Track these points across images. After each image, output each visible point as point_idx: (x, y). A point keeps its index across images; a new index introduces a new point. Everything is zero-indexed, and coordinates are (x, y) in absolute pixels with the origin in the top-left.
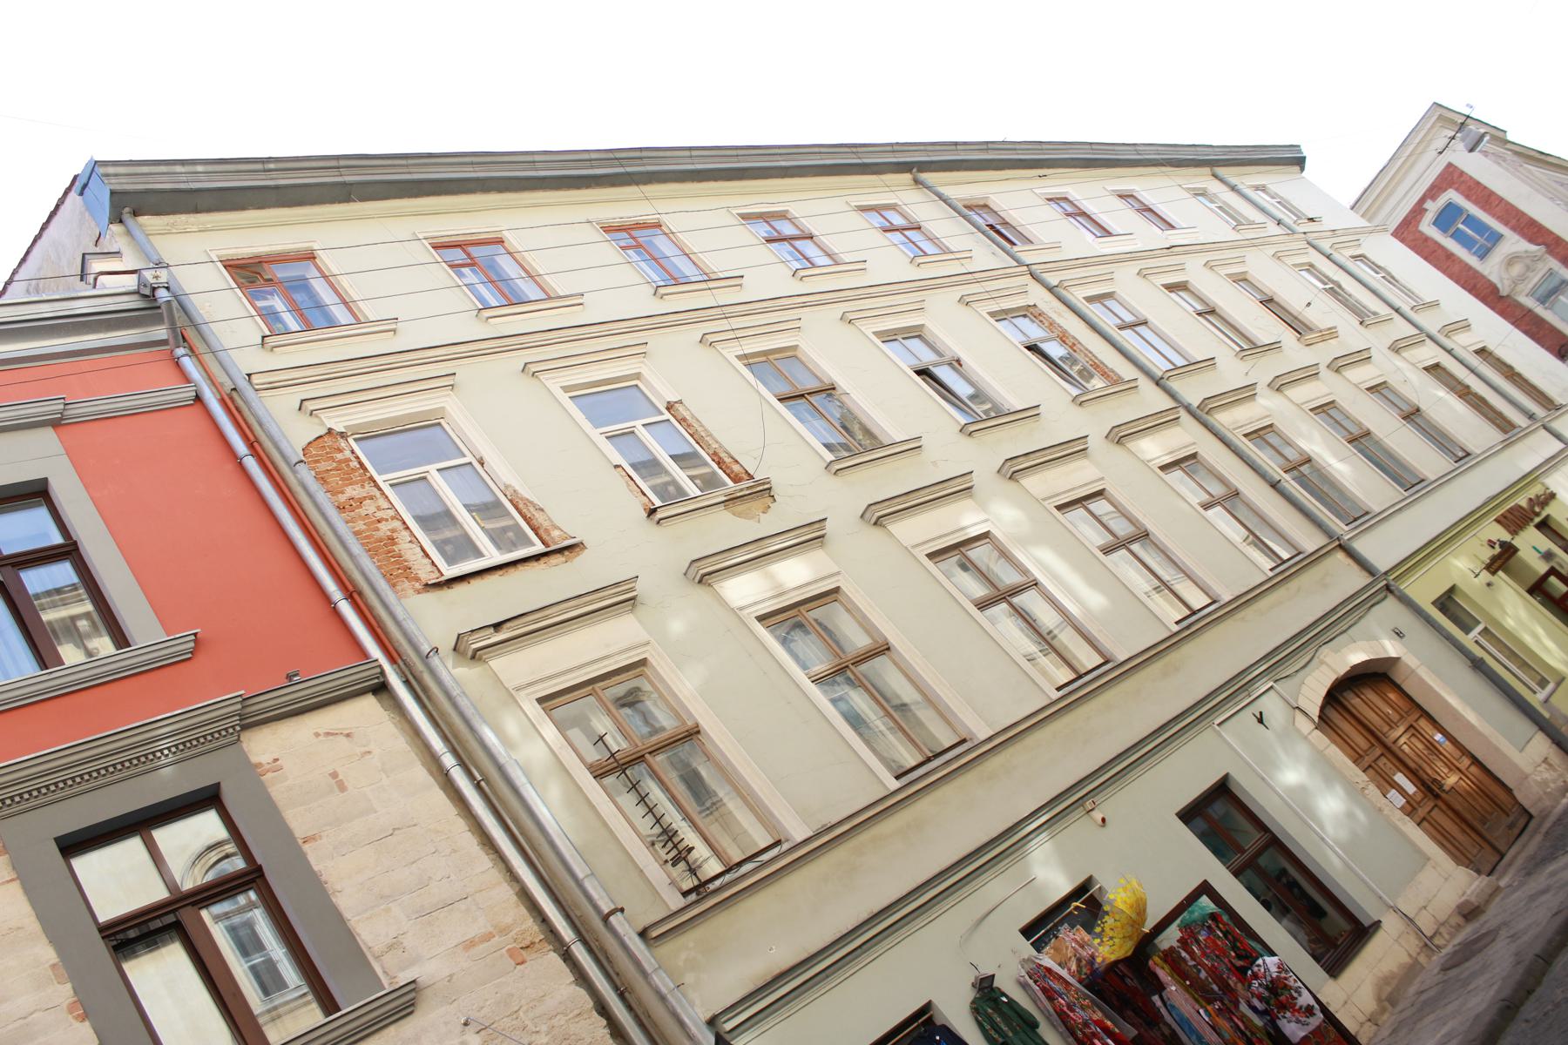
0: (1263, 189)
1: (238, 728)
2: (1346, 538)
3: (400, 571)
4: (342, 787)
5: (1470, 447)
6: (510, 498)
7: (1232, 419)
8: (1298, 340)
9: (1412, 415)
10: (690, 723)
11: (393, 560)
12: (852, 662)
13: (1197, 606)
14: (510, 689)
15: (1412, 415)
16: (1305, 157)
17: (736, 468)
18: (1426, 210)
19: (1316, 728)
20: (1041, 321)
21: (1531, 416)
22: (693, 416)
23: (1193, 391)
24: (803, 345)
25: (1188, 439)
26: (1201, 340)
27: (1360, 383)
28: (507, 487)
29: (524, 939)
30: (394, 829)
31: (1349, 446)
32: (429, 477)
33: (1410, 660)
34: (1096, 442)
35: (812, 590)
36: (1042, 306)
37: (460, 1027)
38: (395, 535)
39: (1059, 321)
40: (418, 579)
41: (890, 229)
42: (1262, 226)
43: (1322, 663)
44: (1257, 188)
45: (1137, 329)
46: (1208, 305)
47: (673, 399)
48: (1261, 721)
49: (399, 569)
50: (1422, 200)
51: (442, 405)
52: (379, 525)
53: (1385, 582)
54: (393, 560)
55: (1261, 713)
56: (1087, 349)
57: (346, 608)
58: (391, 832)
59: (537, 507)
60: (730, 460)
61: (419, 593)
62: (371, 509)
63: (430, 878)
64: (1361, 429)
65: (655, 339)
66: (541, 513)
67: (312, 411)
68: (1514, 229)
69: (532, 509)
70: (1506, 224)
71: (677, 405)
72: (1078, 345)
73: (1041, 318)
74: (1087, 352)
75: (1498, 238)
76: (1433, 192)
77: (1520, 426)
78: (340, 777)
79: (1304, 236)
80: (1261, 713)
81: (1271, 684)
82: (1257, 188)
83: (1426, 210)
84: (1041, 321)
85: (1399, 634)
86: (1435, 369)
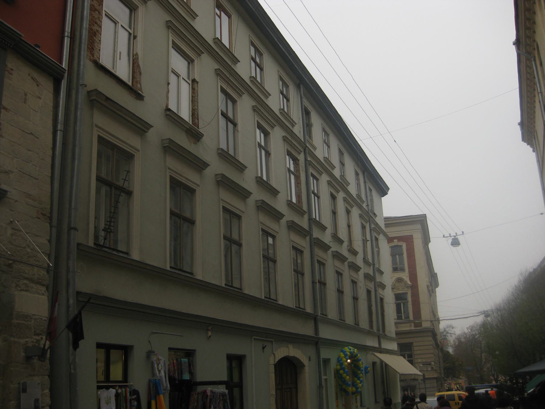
0: (371, 190)
1: (11, 46)
2: (319, 318)
3: (90, 47)
4: (25, 102)
5: (360, 324)
6: (134, 58)
7: (319, 253)
8: (347, 246)
9: (355, 299)
10: (131, 189)
11: (91, 41)
12: (271, 259)
13: (271, 297)
14: (94, 123)
15: (355, 299)
16: (388, 194)
17: (196, 121)
18: (393, 242)
19: (274, 365)
20: (296, 167)
21: (378, 330)
22: (197, 91)
23: (316, 233)
24: (196, 62)
25: (304, 245)
26: (327, 220)
27: (380, 294)
28: (137, 54)
29: (44, 211)
30: (31, 133)
31: (291, 248)
32: (117, 25)
33: (307, 369)
34: (283, 221)
35: (191, 185)
36: (300, 162)
37: (540, 213)
38: (97, 33)
39: (301, 172)
40: (93, 56)
41: (282, 93)
42: (363, 202)
43: (288, 347)
44: (370, 189)
45: (229, 124)
46: (335, 209)
47: (197, 80)
48: (263, 348)
49: (90, 46)
50: (395, 238)
51: (139, 6)
52: (95, 24)
53: (317, 340)
54: (91, 41)
55: (266, 346)
56: (301, 189)
57: (67, 41)
58: (29, 132)
59: (140, 71)
60: (196, 116)
61: (90, 61)
62: (96, 17)
63: (31, 161)
64: (342, 289)
65: (205, 57)
66: (139, 74)
67: (255, 109)
68: (409, 271)
69: (138, 70)
70: (409, 268)
71: (196, 82)
72: (300, 185)
73: (297, 166)
74: (300, 190)
75: (403, 270)
76: (400, 239)
77: (374, 330)
78: (27, 97)
79: (370, 217)
80: (266, 346)
81: (273, 340)
82: (370, 189)
83: (393, 242)
84: (296, 167)
85: (310, 360)
86: (369, 292)
